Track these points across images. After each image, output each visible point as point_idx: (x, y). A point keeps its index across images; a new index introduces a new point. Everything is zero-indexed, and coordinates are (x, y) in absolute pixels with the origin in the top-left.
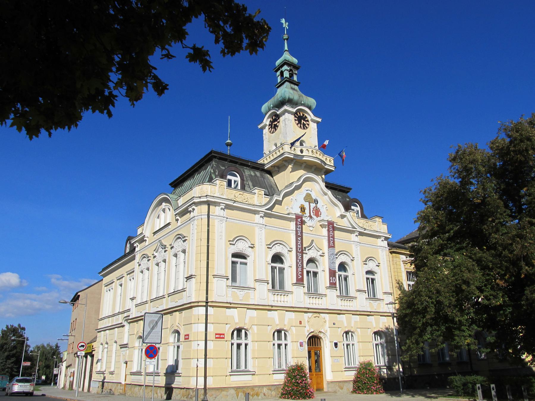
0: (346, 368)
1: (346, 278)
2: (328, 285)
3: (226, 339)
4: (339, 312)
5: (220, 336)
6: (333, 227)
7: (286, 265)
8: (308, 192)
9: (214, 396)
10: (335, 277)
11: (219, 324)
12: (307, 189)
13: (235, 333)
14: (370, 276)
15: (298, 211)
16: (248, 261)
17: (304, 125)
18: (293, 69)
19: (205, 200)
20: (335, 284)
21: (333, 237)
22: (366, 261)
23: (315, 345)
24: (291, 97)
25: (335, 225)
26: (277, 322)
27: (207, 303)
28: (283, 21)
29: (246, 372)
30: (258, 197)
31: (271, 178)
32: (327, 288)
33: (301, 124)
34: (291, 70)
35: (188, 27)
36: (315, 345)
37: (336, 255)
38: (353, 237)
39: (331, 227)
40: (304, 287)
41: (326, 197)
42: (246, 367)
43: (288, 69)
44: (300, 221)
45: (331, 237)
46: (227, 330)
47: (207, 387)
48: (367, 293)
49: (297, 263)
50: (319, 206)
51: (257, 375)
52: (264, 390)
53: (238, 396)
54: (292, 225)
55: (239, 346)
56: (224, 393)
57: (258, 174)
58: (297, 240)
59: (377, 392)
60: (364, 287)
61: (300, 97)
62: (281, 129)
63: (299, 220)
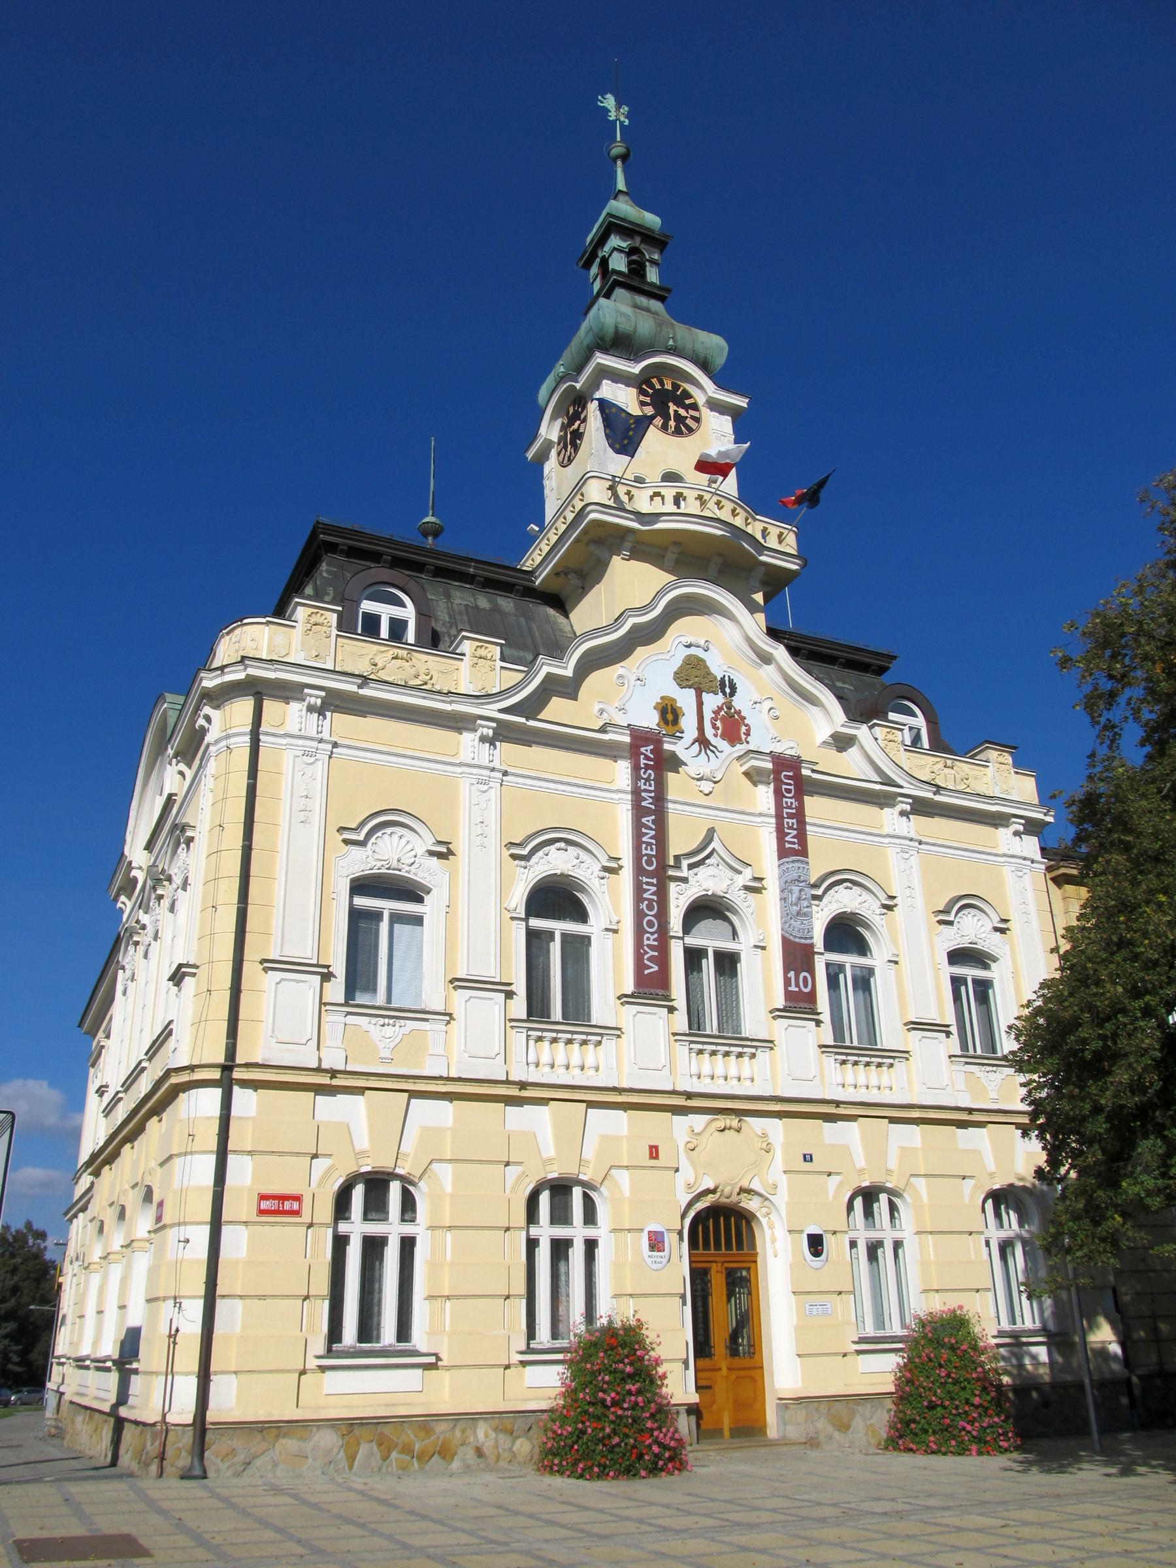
0: (862, 1340)
1: (863, 982)
2: (780, 1002)
3: (306, 1217)
4: (831, 1112)
5: (279, 1206)
6: (799, 780)
7: (594, 928)
8: (693, 651)
9: (241, 1457)
10: (811, 971)
11: (281, 1154)
12: (684, 640)
13: (545, 1199)
14: (970, 972)
15: (650, 720)
16: (429, 908)
17: (680, 419)
18: (643, 247)
19: (241, 676)
20: (812, 997)
21: (800, 815)
22: (946, 911)
23: (729, 1246)
24: (625, 327)
25: (805, 772)
26: (549, 1149)
28: (609, 102)
29: (403, 1352)
30: (476, 669)
31: (561, 619)
32: (777, 1014)
33: (666, 418)
34: (633, 251)
36: (729, 1246)
37: (815, 886)
38: (890, 819)
39: (791, 779)
40: (671, 1010)
41: (770, 669)
42: (404, 1332)
43: (624, 245)
44: (651, 755)
45: (790, 816)
46: (319, 1184)
47: (211, 1416)
48: (955, 1036)
49: (639, 915)
50: (738, 702)
51: (448, 1368)
52: (481, 1434)
53: (351, 1458)
54: (622, 771)
55: (560, 1248)
56: (290, 1444)
57: (507, 604)
58: (638, 827)
59: (985, 1445)
60: (942, 1014)
61: (660, 325)
62: (590, 442)
63: (647, 750)
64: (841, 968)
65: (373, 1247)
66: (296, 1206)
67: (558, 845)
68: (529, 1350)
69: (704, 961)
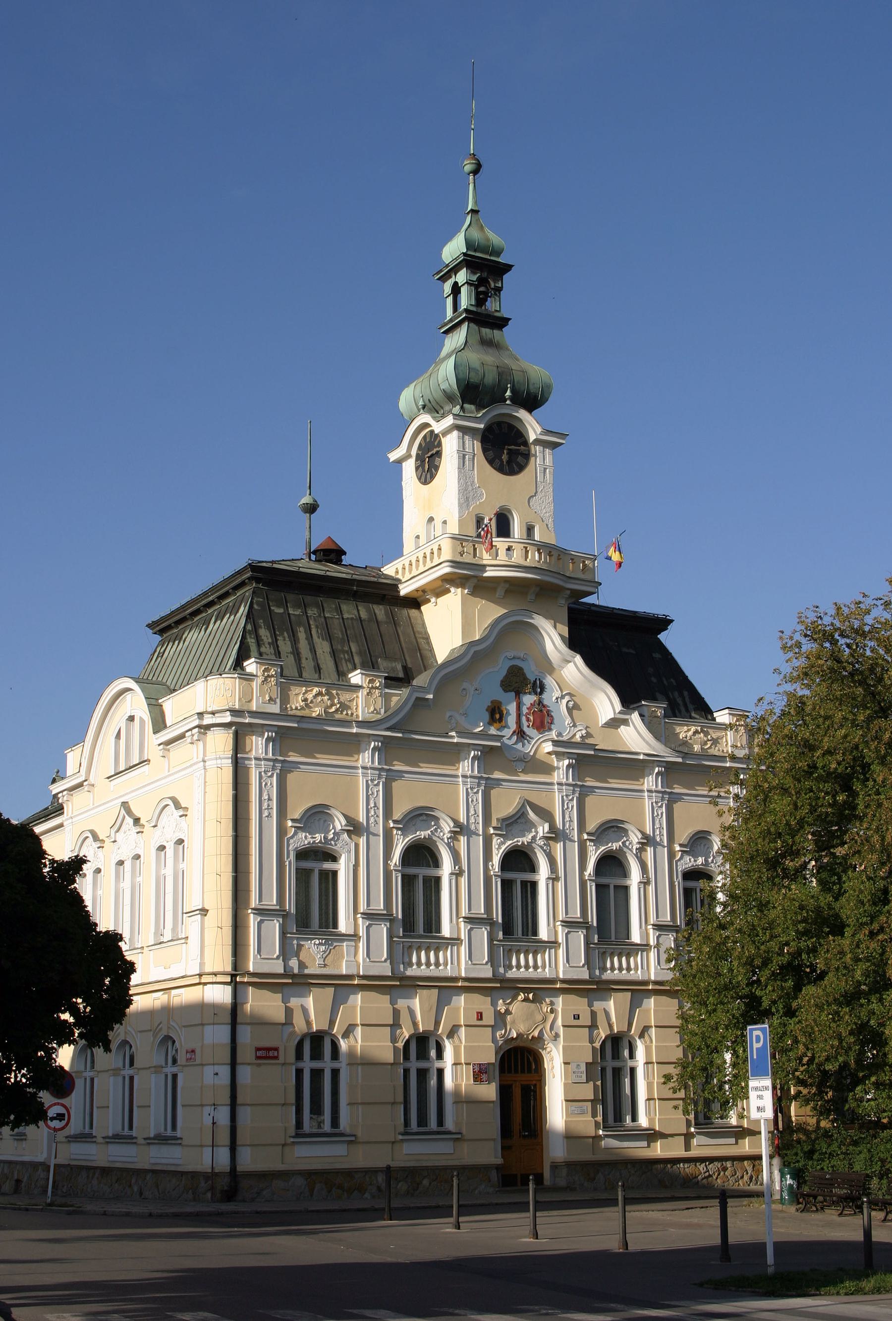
3: (281, 1060)
27: (233, 976)
35: (66, 1046)
42: (440, 1122)
57: (380, 611)
64: (415, 877)
65: (317, 1074)
66: (276, 1054)
67: (421, 818)
68: (297, 1135)
69: (514, 888)
